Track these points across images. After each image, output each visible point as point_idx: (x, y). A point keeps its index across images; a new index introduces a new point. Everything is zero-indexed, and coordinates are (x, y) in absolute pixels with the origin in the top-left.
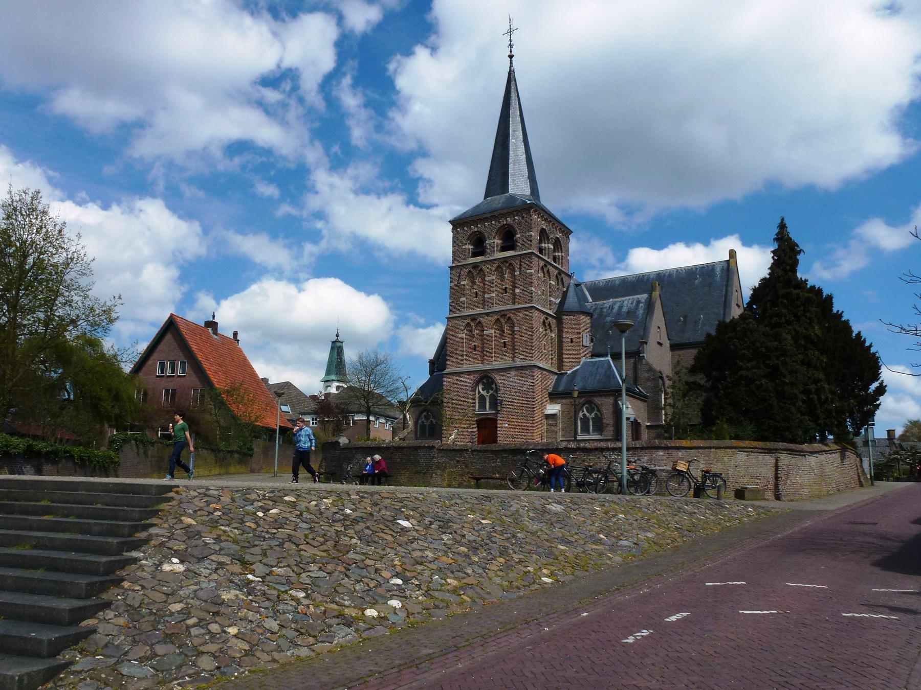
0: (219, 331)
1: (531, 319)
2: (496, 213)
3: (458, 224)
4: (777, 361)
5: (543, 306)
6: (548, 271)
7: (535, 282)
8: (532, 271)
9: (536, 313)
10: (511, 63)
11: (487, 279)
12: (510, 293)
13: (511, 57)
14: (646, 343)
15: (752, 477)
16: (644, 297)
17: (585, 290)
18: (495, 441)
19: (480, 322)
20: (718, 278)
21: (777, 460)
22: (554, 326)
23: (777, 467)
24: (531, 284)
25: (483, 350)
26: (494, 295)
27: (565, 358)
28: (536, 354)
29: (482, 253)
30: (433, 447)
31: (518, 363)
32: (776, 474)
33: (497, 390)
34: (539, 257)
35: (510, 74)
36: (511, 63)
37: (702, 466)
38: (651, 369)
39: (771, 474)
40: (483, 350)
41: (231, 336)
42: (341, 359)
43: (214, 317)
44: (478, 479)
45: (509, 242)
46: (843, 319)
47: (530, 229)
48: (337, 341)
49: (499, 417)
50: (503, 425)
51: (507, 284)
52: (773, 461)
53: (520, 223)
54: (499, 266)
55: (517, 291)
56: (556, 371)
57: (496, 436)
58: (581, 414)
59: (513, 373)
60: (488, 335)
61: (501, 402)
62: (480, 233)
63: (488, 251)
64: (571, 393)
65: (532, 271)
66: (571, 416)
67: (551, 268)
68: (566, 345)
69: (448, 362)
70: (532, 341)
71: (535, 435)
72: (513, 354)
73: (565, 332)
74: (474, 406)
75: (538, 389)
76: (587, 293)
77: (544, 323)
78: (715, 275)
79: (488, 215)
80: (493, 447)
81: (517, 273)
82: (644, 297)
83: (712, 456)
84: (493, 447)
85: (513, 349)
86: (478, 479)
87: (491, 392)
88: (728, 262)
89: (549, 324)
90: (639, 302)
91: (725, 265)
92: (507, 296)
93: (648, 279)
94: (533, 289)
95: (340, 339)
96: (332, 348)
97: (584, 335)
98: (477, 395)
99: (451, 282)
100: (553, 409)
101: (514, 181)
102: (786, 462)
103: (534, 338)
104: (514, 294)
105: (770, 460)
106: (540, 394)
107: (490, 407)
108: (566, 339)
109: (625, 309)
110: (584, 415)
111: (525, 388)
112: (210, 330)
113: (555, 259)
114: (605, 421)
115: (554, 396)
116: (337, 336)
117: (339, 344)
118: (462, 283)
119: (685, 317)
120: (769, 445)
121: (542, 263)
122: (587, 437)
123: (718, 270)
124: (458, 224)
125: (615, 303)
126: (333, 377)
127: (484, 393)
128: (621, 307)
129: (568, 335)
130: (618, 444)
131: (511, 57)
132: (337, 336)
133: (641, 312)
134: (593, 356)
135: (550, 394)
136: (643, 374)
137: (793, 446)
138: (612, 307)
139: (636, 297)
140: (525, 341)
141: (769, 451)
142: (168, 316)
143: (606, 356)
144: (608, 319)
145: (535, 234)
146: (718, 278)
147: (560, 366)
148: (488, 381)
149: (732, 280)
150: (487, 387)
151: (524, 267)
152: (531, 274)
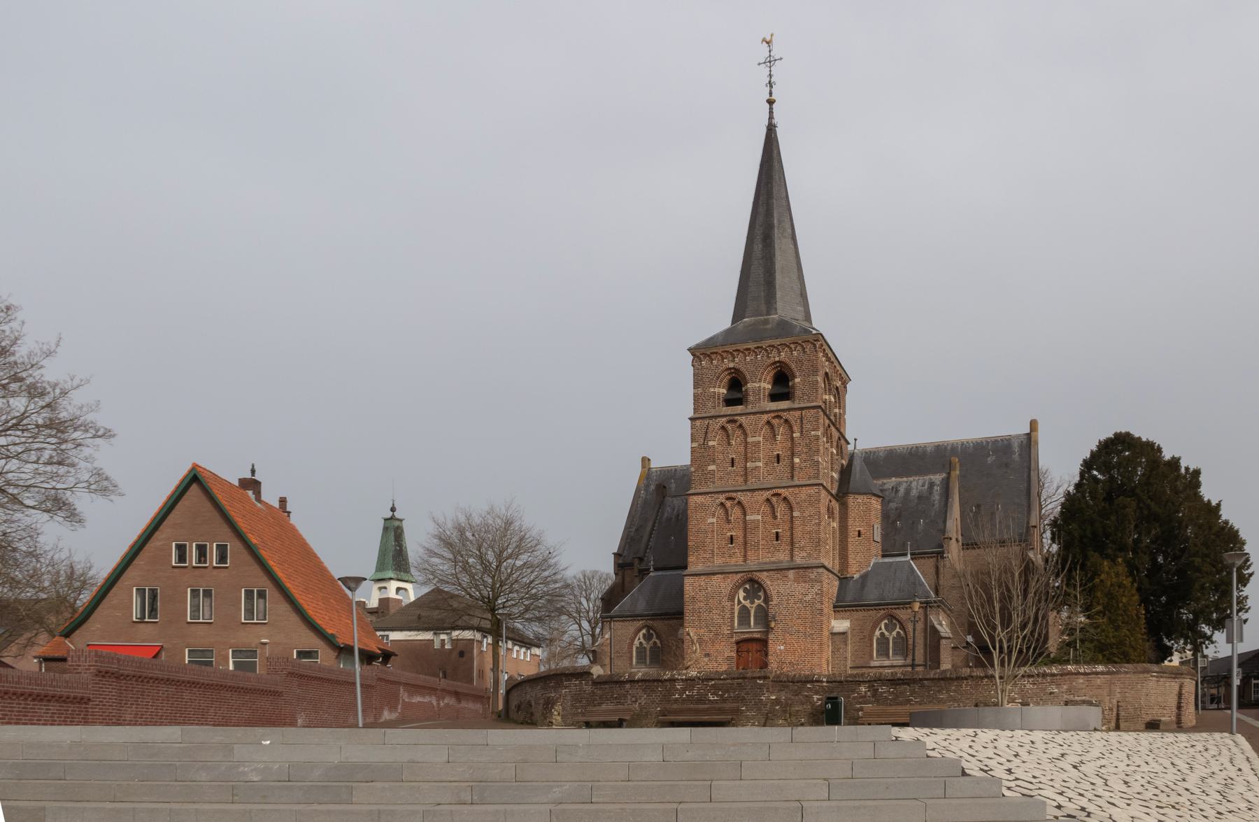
0: (263, 498)
4: (1120, 566)
10: (771, 112)
11: (750, 440)
12: (785, 462)
13: (771, 102)
16: (938, 478)
20: (1016, 457)
21: (1181, 687)
22: (837, 515)
25: (745, 543)
26: (760, 464)
27: (851, 557)
29: (738, 402)
32: (1179, 703)
36: (771, 112)
39: (1173, 702)
40: (745, 543)
41: (276, 505)
42: (400, 546)
43: (253, 472)
48: (392, 518)
49: (771, 636)
50: (777, 647)
51: (780, 447)
52: (1177, 688)
54: (768, 423)
55: (797, 460)
58: (877, 633)
59: (791, 574)
60: (753, 521)
61: (774, 617)
62: (737, 370)
63: (751, 398)
66: (864, 635)
67: (743, 419)
68: (852, 539)
69: (691, 559)
70: (818, 532)
72: (792, 550)
73: (850, 522)
74: (732, 621)
78: (1013, 453)
81: (796, 435)
82: (938, 478)
84: (460, 686)
85: (792, 543)
88: (1029, 435)
90: (932, 485)
92: (782, 467)
93: (925, 452)
95: (397, 515)
96: (386, 529)
98: (737, 608)
99: (693, 440)
100: (841, 625)
104: (792, 463)
107: (756, 623)
108: (852, 533)
109: (914, 493)
110: (882, 634)
111: (808, 598)
112: (250, 493)
115: (840, 607)
116: (393, 509)
117: (397, 523)
118: (711, 443)
119: (978, 506)
122: (887, 663)
125: (900, 484)
126: (390, 574)
127: (747, 603)
128: (908, 491)
129: (854, 525)
131: (771, 102)
132: (393, 509)
133: (936, 497)
134: (883, 556)
135: (835, 607)
138: (895, 489)
139: (927, 478)
140: (809, 533)
142: (189, 467)
143: (905, 555)
146: (1016, 457)
150: (750, 595)
151: (807, 426)
152: (817, 438)
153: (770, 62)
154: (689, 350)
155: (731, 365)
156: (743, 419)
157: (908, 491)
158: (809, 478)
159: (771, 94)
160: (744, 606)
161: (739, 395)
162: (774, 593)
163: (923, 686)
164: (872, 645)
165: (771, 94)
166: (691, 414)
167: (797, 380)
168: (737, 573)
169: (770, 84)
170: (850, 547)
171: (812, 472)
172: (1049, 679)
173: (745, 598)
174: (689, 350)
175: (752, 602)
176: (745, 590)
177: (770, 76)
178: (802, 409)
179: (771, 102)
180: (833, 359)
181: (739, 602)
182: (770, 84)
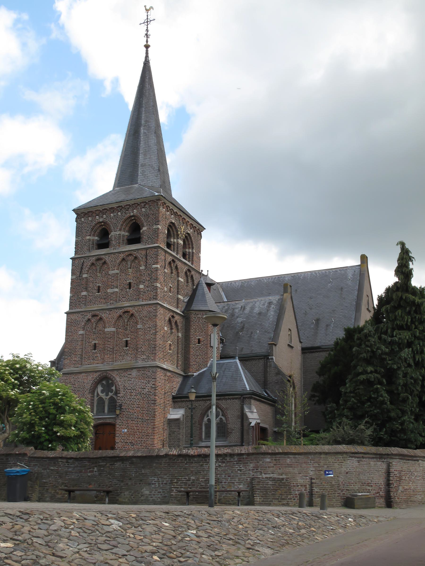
1: (156, 316)
2: (122, 204)
3: (83, 214)
5: (169, 303)
6: (176, 267)
7: (161, 278)
8: (158, 266)
9: (161, 311)
10: (147, 53)
13: (147, 47)
14: (276, 345)
15: (363, 484)
17: (221, 290)
18: (113, 448)
19: (101, 319)
23: (388, 473)
24: (156, 280)
28: (160, 354)
30: (25, 455)
31: (140, 364)
33: (116, 393)
34: (166, 252)
35: (145, 64)
36: (147, 53)
37: (312, 473)
38: (279, 372)
39: (382, 481)
44: (70, 492)
45: (135, 236)
46: (396, 280)
47: (157, 222)
50: (122, 431)
52: (384, 466)
53: (147, 216)
56: (182, 373)
57: (114, 443)
59: (134, 373)
61: (121, 406)
62: (105, 223)
64: (188, 397)
65: (158, 266)
70: (155, 340)
71: (156, 442)
73: (192, 332)
75: (160, 392)
76: (223, 294)
77: (170, 320)
79: (115, 206)
80: (109, 453)
82: (274, 299)
83: (322, 462)
86: (70, 492)
87: (110, 394)
89: (176, 322)
91: (357, 272)
94: (158, 285)
97: (212, 336)
98: (96, 399)
100: (177, 414)
101: (143, 171)
102: (398, 468)
103: (158, 337)
105: (381, 466)
106: (163, 397)
108: (194, 340)
109: (256, 310)
113: (184, 256)
114: (230, 426)
115: (178, 399)
118: (85, 276)
120: (382, 450)
121: (169, 259)
123: (350, 276)
124: (83, 214)
127: (103, 395)
128: (252, 308)
129: (195, 336)
130: (207, 444)
135: (174, 398)
136: (272, 377)
137: (405, 451)
138: (243, 308)
140: (149, 340)
141: (381, 456)
143: (233, 357)
144: (240, 320)
145: (162, 228)
147: (186, 365)
148: (107, 382)
149: (365, 287)
150: (107, 389)
151: (150, 261)
153: (147, 22)
154: (74, 210)
155: (101, 220)
156: (107, 258)
157: (252, 308)
158: (150, 299)
159: (147, 41)
160: (101, 397)
161: (137, 236)
162: (121, 387)
163: (132, 463)
164: (201, 429)
165: (147, 41)
166: (73, 255)
167: (144, 229)
168: (96, 372)
169: (147, 35)
170: (192, 351)
171: (153, 294)
172: (236, 458)
173: (102, 392)
174: (74, 210)
175: (107, 395)
176: (103, 385)
177: (147, 30)
178: (146, 249)
179: (147, 47)
180: (180, 213)
181: (98, 395)
182: (147, 35)
